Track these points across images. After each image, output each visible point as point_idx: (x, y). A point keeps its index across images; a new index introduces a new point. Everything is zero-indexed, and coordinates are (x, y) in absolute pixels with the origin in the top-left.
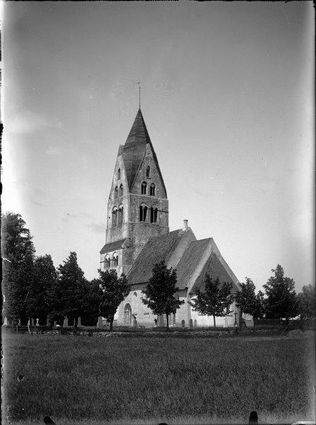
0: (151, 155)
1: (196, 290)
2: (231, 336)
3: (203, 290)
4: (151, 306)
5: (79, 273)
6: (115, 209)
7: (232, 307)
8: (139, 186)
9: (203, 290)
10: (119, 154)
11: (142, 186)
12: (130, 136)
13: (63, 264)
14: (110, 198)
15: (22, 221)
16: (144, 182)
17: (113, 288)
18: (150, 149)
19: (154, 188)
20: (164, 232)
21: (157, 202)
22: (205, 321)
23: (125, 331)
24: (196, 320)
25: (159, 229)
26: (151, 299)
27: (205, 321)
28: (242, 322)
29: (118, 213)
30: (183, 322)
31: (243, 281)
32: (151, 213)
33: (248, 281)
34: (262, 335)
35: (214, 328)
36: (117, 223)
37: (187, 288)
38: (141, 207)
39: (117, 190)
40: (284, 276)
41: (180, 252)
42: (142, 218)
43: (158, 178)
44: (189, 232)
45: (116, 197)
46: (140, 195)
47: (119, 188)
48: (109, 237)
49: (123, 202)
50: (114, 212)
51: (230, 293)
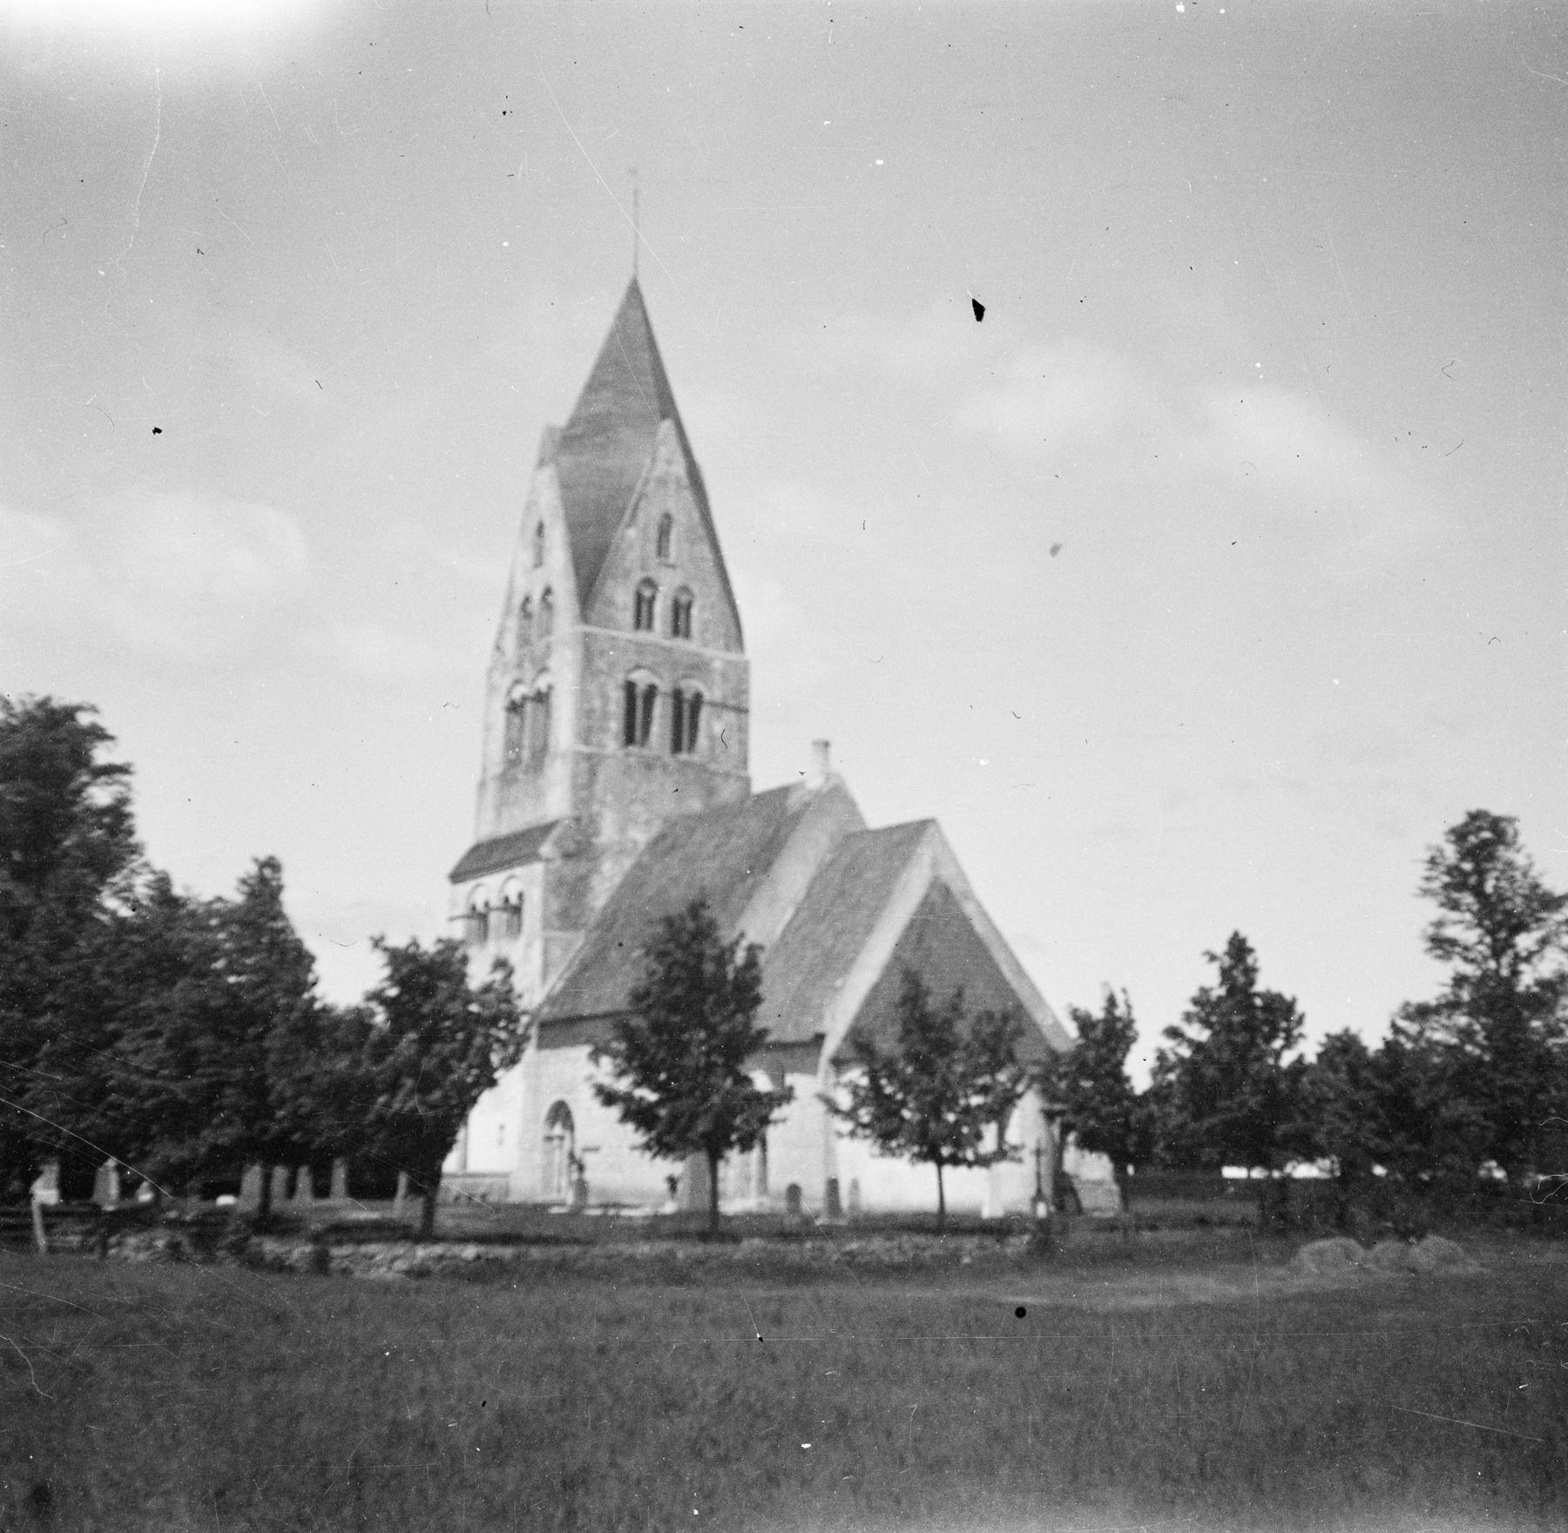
0: (679, 468)
1: (860, 1046)
2: (1021, 1266)
3: (888, 1044)
4: (638, 1115)
5: (292, 961)
6: (518, 693)
7: (1026, 1121)
8: (622, 596)
9: (888, 1044)
10: (542, 463)
11: (639, 598)
12: (594, 386)
13: (1373, 1040)
14: (498, 648)
15: (98, 734)
16: (649, 582)
17: (441, 1024)
18: (673, 441)
19: (689, 606)
20: (728, 792)
21: (698, 667)
22: (898, 1183)
23: (505, 1239)
24: (855, 1185)
25: (706, 779)
26: (637, 1084)
27: (898, 1183)
28: (1062, 1188)
29: (527, 708)
30: (794, 1192)
31: (208, 877)
32: (666, 717)
33: (1294, 1000)
34: (1171, 1259)
35: (941, 1223)
36: (526, 754)
37: (819, 1038)
38: (630, 687)
39: (531, 614)
40: (1260, 986)
41: (794, 875)
42: (632, 733)
43: (709, 565)
44: (836, 795)
45: (524, 641)
46: (627, 634)
47: (535, 605)
48: (489, 815)
49: (552, 663)
50: (514, 708)
51: (1011, 1057)
